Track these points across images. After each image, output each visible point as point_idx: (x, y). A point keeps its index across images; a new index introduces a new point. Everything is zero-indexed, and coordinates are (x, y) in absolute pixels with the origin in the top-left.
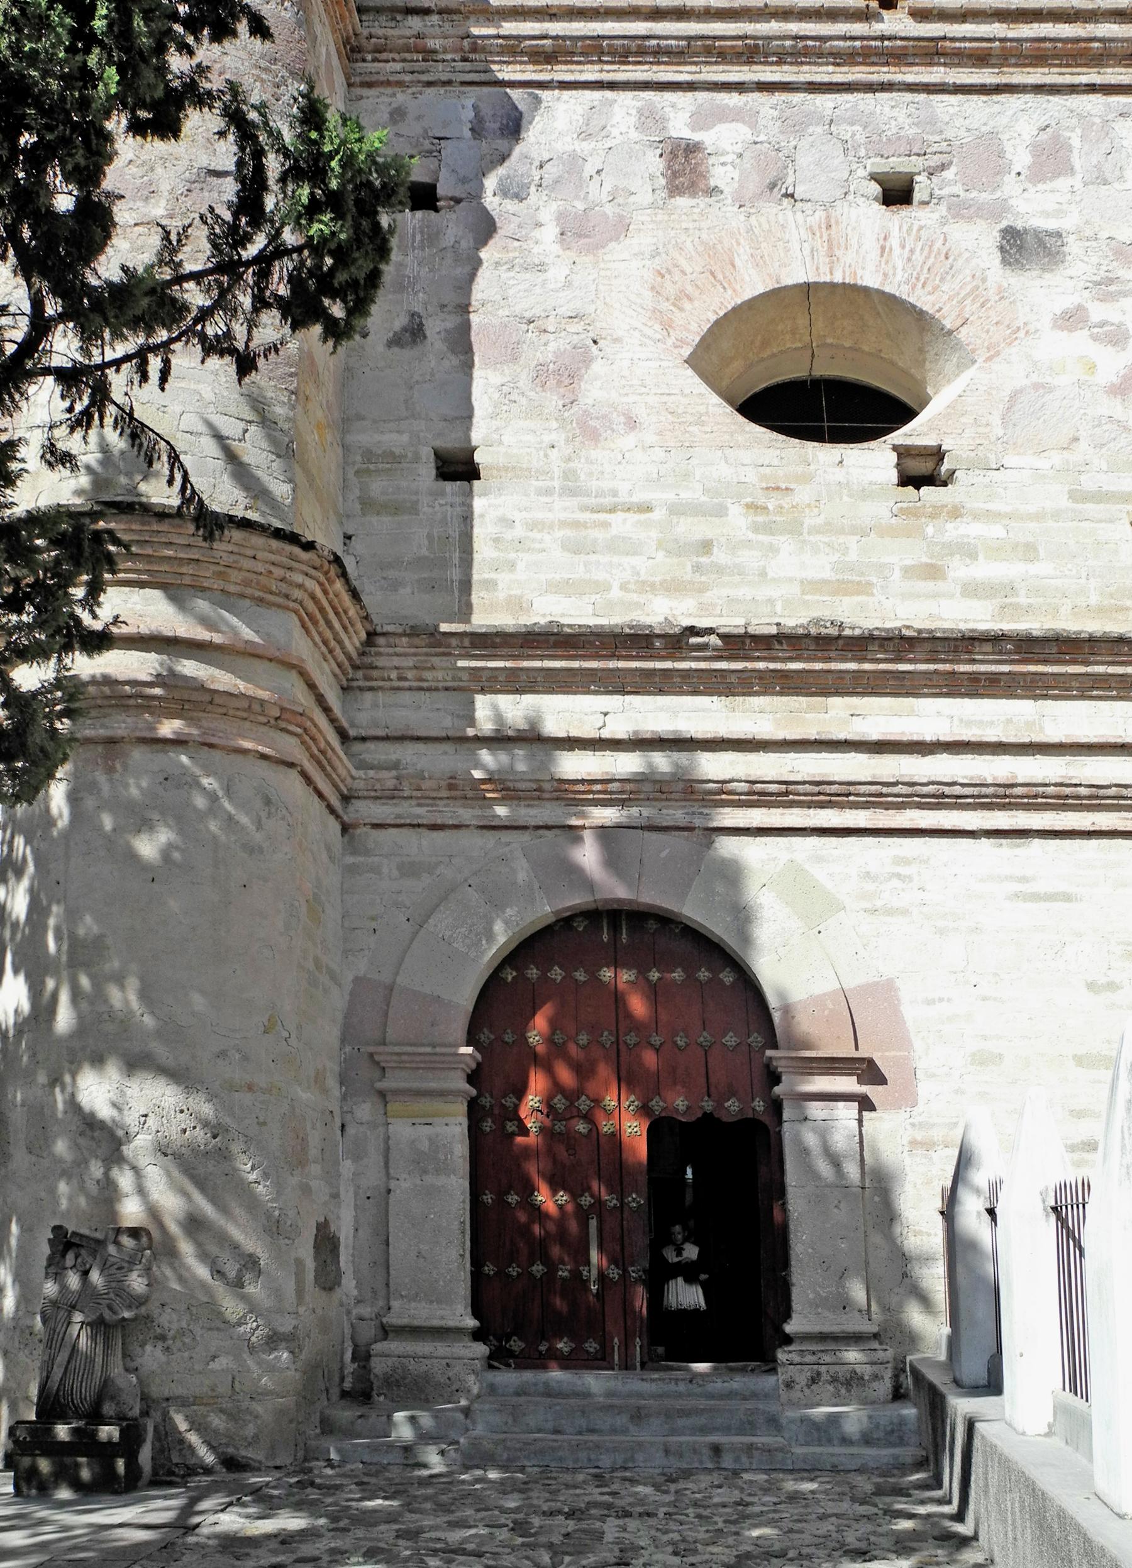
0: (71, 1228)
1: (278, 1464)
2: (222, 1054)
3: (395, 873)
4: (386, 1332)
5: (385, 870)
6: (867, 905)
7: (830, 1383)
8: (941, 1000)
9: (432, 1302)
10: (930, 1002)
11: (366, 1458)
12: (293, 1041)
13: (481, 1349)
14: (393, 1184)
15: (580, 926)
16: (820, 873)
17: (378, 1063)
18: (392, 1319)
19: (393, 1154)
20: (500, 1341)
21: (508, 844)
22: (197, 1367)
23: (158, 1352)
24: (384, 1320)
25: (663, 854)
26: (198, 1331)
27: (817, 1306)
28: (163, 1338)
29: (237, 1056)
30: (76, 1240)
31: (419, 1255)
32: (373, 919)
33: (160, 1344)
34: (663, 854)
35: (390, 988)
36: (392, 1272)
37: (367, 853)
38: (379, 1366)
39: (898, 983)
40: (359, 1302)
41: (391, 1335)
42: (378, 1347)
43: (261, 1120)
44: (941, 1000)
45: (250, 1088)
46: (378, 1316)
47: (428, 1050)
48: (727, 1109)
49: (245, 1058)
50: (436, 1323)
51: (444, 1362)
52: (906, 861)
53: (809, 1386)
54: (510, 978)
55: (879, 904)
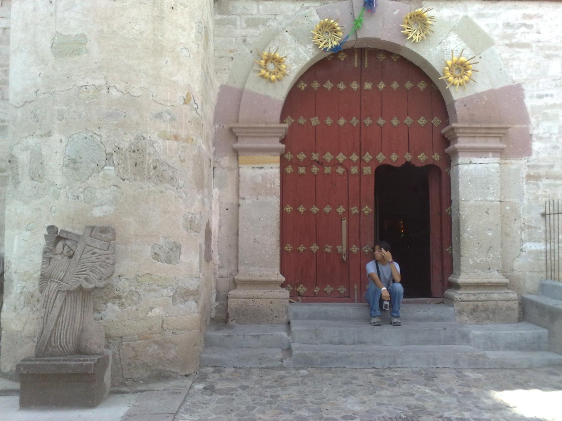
0: (60, 227)
1: (187, 373)
2: (159, 116)
3: (244, 25)
4: (235, 284)
5: (238, 23)
6: (507, 42)
7: (484, 311)
8: (547, 95)
9: (262, 267)
10: (541, 97)
11: (236, 365)
12: (199, 110)
13: (286, 293)
14: (241, 202)
15: (342, 57)
16: (481, 23)
17: (234, 134)
18: (240, 277)
19: (242, 185)
20: (293, 287)
21: (308, 8)
22: (140, 315)
23: (116, 307)
24: (236, 277)
25: (396, 13)
26: (141, 291)
27: (475, 268)
28: (119, 297)
29: (168, 117)
30: (64, 235)
31: (255, 240)
32: (231, 51)
33: (117, 301)
34: (396, 13)
35: (241, 92)
36: (240, 251)
37: (228, 13)
38: (232, 303)
39: (524, 86)
40: (220, 267)
41: (238, 287)
42: (233, 293)
43: (182, 158)
44: (547, 95)
45: (176, 138)
46: (231, 274)
47: (264, 125)
48: (419, 160)
49: (173, 119)
50: (265, 278)
51: (269, 301)
52: (530, 17)
53: (471, 314)
54: (303, 88)
55: (514, 41)
